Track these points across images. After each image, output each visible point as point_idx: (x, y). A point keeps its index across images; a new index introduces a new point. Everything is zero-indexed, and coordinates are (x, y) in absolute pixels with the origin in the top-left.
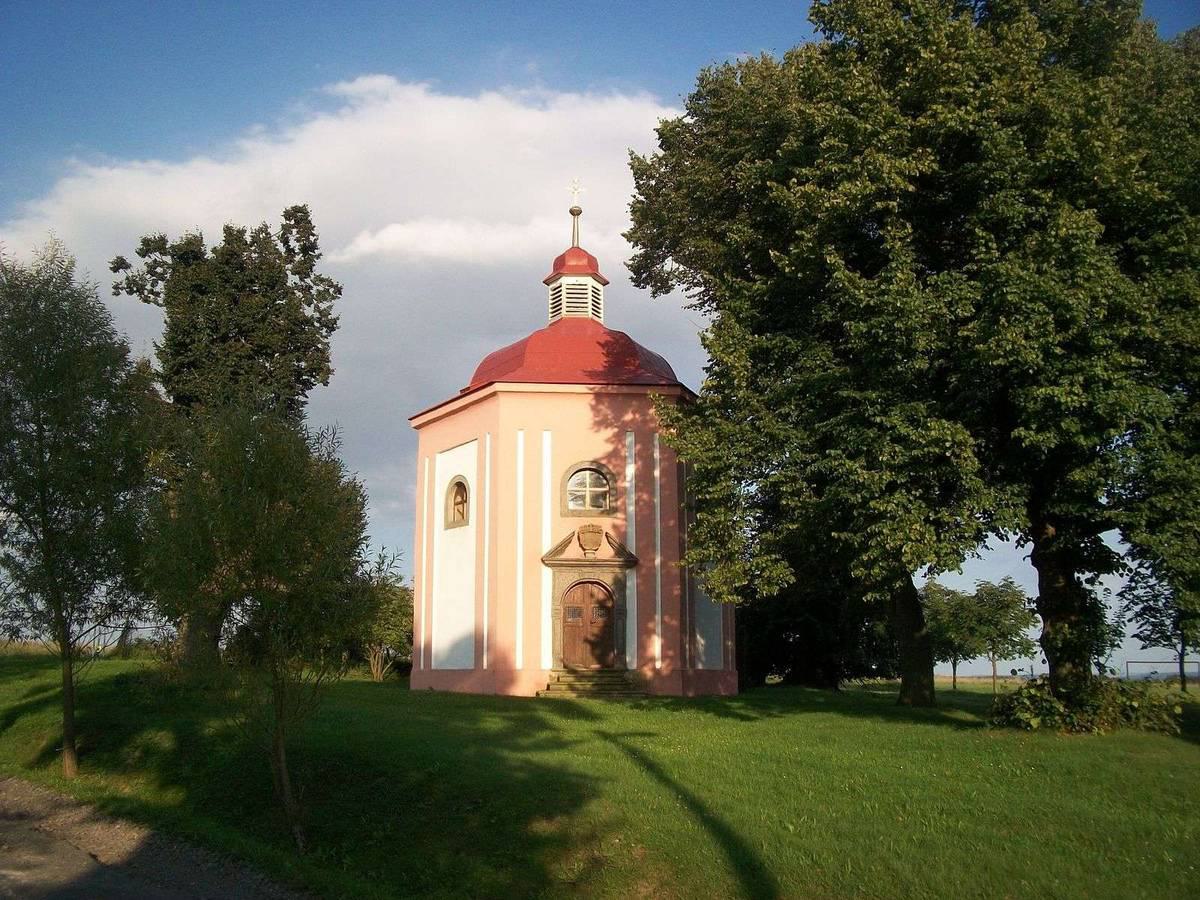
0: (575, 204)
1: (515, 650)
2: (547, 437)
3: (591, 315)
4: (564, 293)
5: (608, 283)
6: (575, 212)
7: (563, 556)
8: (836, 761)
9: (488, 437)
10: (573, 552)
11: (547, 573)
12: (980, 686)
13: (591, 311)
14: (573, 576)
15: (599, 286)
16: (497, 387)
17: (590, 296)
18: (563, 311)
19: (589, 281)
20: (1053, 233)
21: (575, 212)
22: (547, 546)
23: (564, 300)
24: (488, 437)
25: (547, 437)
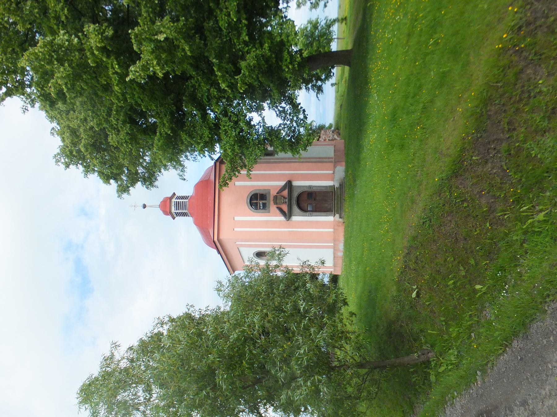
0: (142, 204)
1: (276, 186)
2: (237, 218)
3: (187, 200)
4: (177, 211)
5: (174, 193)
6: (145, 206)
7: (287, 212)
8: (482, 241)
9: (237, 243)
10: (285, 208)
11: (295, 218)
12: (347, 85)
13: (186, 200)
14: (295, 209)
15: (176, 197)
16: (216, 239)
17: (181, 200)
18: (186, 211)
19: (174, 200)
20: (526, 384)
21: (145, 206)
22: (282, 218)
23: (181, 211)
24: (237, 243)
25: (237, 218)
